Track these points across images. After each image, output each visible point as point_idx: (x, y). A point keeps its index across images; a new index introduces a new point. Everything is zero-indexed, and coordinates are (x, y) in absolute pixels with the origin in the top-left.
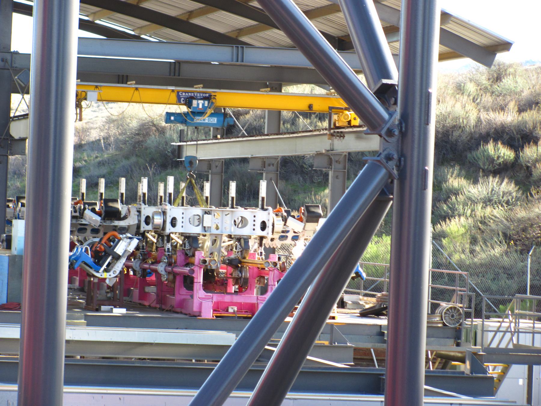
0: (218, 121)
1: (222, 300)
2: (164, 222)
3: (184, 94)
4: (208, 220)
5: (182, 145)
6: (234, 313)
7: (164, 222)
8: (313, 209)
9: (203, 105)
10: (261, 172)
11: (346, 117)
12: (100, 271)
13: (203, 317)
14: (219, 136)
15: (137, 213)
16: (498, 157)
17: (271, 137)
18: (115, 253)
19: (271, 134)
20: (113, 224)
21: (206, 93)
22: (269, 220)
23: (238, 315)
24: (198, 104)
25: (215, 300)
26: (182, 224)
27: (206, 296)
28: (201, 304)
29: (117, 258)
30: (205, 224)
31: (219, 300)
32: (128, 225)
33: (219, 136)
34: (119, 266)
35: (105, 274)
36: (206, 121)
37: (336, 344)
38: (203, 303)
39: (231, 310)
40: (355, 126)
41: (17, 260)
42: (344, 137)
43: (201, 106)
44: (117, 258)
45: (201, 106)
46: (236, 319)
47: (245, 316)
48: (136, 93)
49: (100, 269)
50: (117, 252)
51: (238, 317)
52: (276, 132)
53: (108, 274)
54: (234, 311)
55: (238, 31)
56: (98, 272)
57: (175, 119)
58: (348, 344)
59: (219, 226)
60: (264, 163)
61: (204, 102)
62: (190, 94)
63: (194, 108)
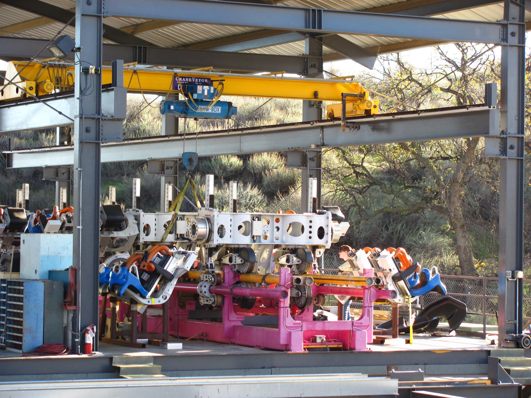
0: (222, 110)
1: (312, 329)
2: (211, 231)
3: (180, 79)
4: (259, 228)
5: (12, 154)
6: (322, 343)
7: (211, 231)
8: (17, 215)
9: (209, 91)
10: (54, 180)
11: (369, 104)
12: (147, 297)
13: (293, 352)
14: (66, 143)
15: (136, 222)
16: (231, 165)
17: (171, 138)
18: (166, 271)
19: (171, 136)
20: (111, 235)
21: (204, 79)
22: (328, 226)
23: (329, 346)
24: (203, 91)
25: (304, 328)
26: (231, 234)
27: (294, 324)
28: (290, 334)
29: (167, 278)
30: (255, 234)
31: (309, 329)
32: (129, 235)
33: (66, 143)
34: (170, 289)
35: (153, 299)
36: (210, 111)
37: (501, 383)
38: (292, 334)
39: (319, 341)
40: (374, 116)
41: (55, 286)
42: (359, 128)
43: (206, 93)
44: (167, 278)
45: (206, 93)
46: (329, 351)
47: (336, 346)
48: (135, 76)
49: (147, 294)
50: (168, 270)
51: (330, 348)
52: (173, 133)
53: (157, 300)
54: (322, 341)
55: (133, 27)
56: (144, 297)
57: (175, 109)
58: (514, 383)
59: (268, 234)
60: (163, 166)
61: (210, 89)
62: (187, 79)
63: (199, 95)
